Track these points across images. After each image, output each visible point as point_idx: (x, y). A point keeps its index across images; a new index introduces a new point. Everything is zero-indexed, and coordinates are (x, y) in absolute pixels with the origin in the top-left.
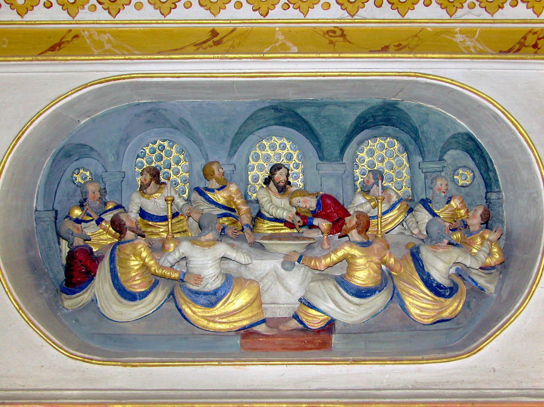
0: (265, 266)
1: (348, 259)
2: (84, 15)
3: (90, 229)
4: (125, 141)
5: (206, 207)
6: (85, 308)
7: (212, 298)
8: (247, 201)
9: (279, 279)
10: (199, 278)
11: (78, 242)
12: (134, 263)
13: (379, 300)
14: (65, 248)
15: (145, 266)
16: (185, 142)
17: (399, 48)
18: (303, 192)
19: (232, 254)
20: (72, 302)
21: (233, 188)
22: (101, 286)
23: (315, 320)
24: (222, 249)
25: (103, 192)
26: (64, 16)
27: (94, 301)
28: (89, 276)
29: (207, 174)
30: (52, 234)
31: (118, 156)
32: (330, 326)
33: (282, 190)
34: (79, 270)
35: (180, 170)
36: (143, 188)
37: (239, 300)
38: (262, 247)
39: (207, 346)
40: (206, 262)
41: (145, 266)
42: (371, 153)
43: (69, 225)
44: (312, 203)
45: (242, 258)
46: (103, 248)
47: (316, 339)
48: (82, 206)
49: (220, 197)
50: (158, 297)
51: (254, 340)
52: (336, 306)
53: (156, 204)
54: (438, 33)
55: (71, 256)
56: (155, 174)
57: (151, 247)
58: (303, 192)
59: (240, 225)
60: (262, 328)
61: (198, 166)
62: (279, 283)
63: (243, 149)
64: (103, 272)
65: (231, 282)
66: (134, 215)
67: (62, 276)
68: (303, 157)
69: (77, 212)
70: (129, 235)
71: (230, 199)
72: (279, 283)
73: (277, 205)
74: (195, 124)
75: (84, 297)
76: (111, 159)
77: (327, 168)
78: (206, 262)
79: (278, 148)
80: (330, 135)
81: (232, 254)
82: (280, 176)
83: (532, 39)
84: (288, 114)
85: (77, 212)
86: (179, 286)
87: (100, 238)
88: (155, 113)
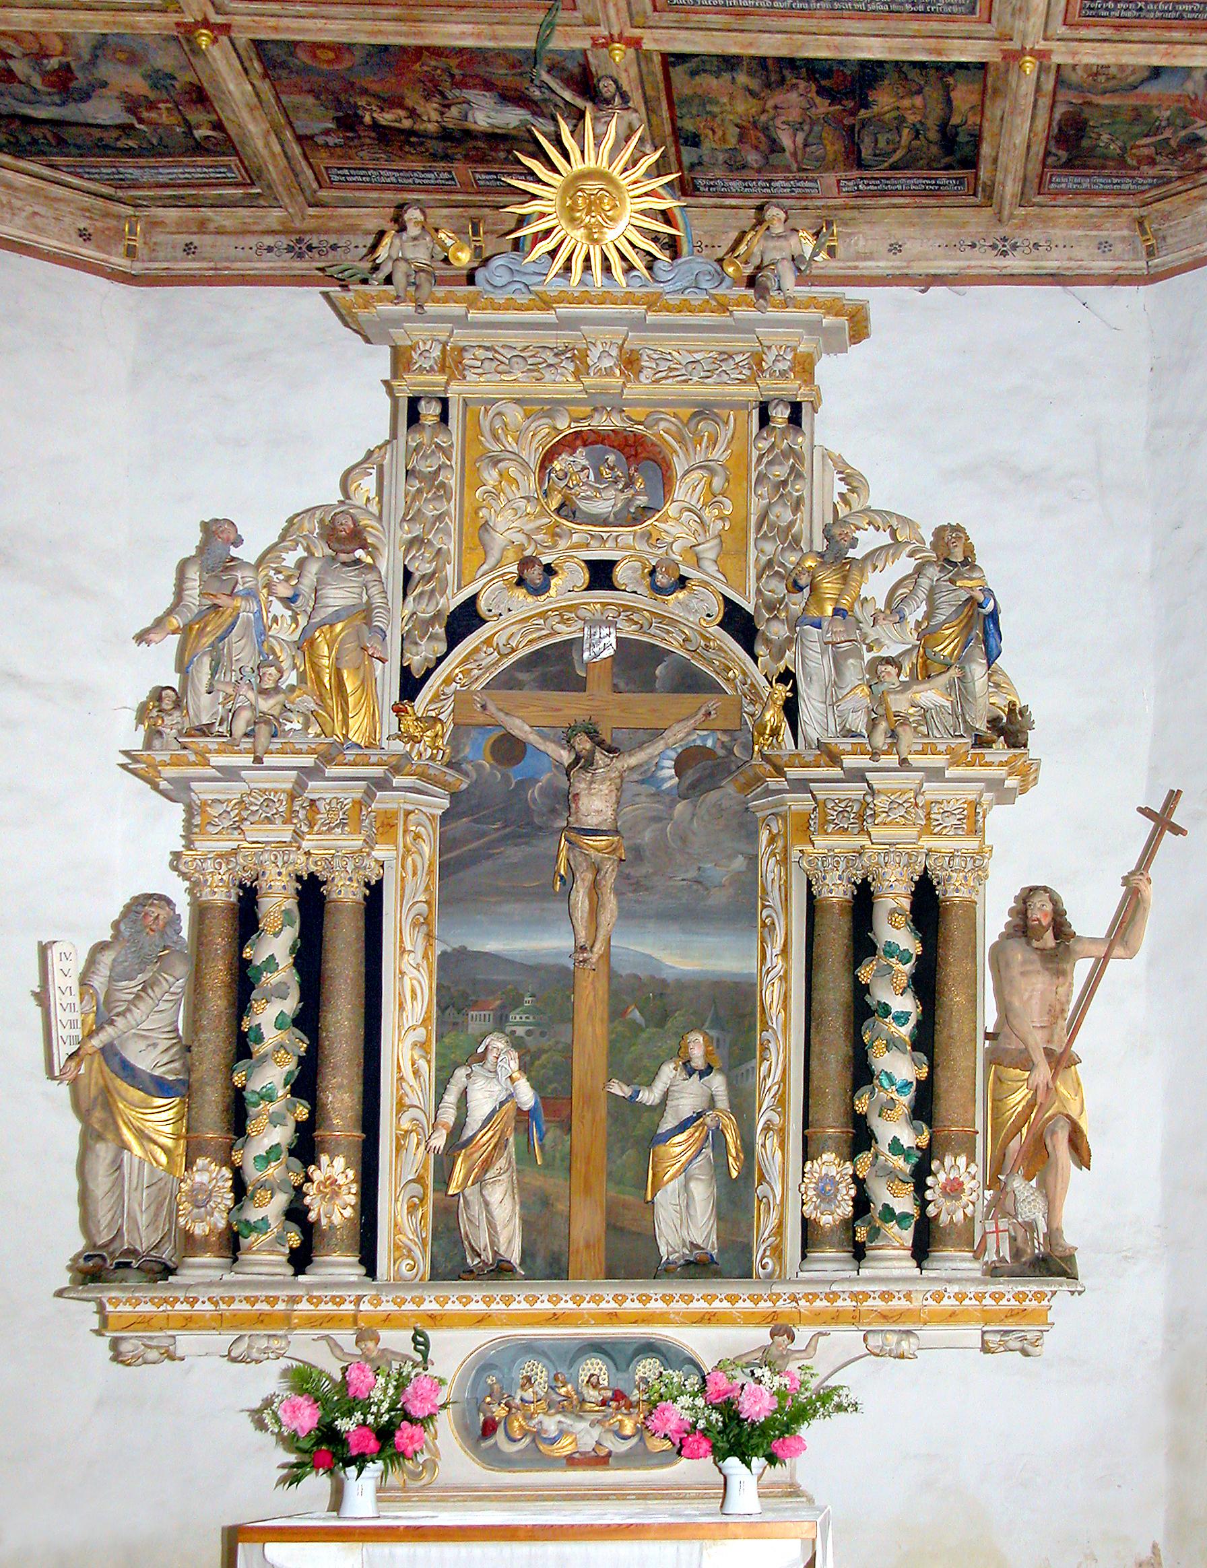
0: (582, 1426)
1: (621, 1421)
2: (494, 1306)
3: (495, 1408)
4: (514, 1362)
5: (554, 1396)
6: (491, 1447)
7: (553, 1441)
8: (577, 1393)
9: (588, 1432)
10: (546, 1431)
11: (489, 1414)
12: (516, 1424)
13: (634, 1440)
14: (482, 1418)
15: (521, 1426)
16: (546, 1361)
17: (643, 1321)
18: (605, 1388)
19: (563, 1419)
20: (486, 1444)
21: (569, 1386)
22: (500, 1435)
23: (603, 1453)
24: (559, 1417)
25: (502, 1388)
26: (484, 1307)
27: (496, 1443)
28: (495, 1429)
29: (556, 1378)
30: (475, 1411)
31: (510, 1369)
32: (610, 1454)
33: (594, 1387)
34: (489, 1428)
35: (542, 1376)
36: (522, 1386)
37: (565, 1441)
38: (581, 1417)
39: (549, 1463)
40: (551, 1424)
41: (521, 1426)
42: (644, 1367)
43: (485, 1406)
44: (610, 1394)
45: (569, 1421)
46: (501, 1418)
47: (600, 1460)
48: (490, 1396)
49: (563, 1391)
50: (527, 1440)
51: (572, 1461)
52: (613, 1445)
53: (529, 1395)
54: (662, 1314)
55: (485, 1423)
56: (529, 1379)
57: (525, 1418)
58: (605, 1388)
59: (575, 1406)
60: (577, 1455)
61: (552, 1375)
62: (586, 1434)
63: (576, 1365)
64: (500, 1431)
65: (562, 1433)
66: (518, 1401)
67: (480, 1432)
68: (608, 1369)
69: (488, 1399)
70: (514, 1410)
71: (568, 1392)
72: (586, 1434)
73: (592, 1395)
74: (550, 1353)
75: (491, 1442)
76: (506, 1370)
77: (620, 1375)
78: (551, 1424)
79: (595, 1366)
80: (833, 1297)
81: (563, 1419)
82: (594, 1379)
83: (707, 1317)
84: (597, 1348)
85: (488, 1399)
86: (537, 1436)
87: (499, 1412)
88: (530, 1348)
